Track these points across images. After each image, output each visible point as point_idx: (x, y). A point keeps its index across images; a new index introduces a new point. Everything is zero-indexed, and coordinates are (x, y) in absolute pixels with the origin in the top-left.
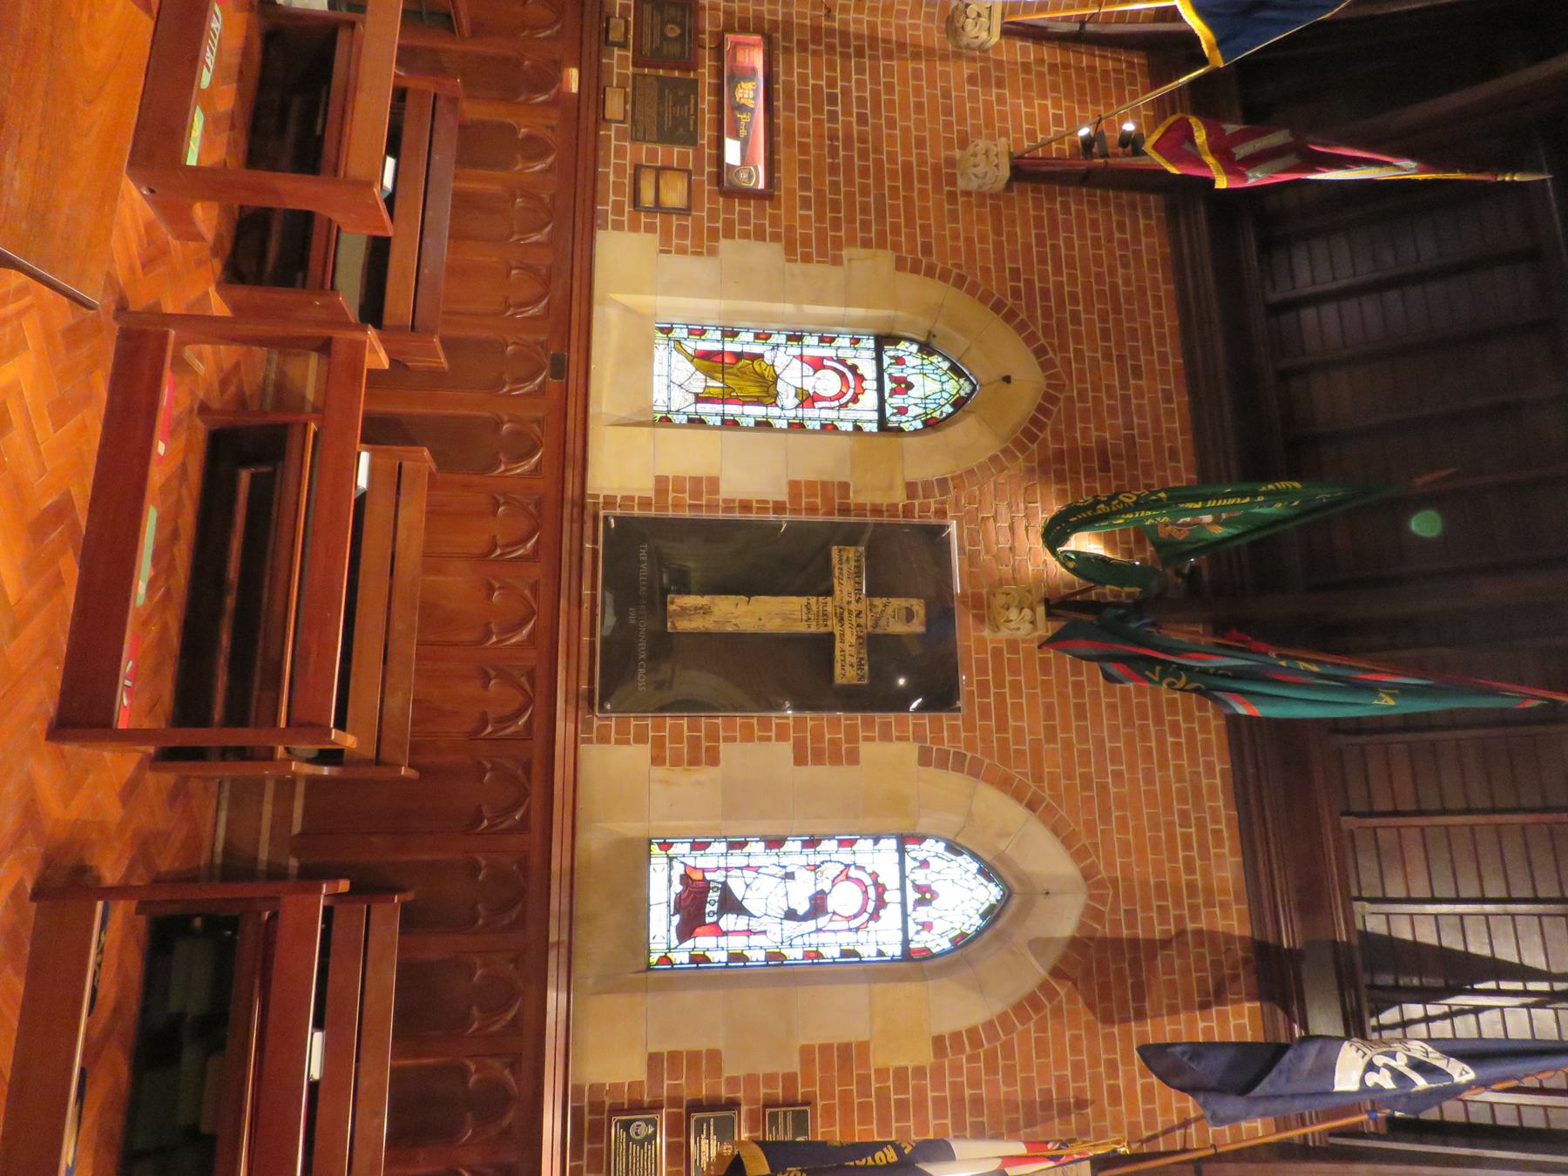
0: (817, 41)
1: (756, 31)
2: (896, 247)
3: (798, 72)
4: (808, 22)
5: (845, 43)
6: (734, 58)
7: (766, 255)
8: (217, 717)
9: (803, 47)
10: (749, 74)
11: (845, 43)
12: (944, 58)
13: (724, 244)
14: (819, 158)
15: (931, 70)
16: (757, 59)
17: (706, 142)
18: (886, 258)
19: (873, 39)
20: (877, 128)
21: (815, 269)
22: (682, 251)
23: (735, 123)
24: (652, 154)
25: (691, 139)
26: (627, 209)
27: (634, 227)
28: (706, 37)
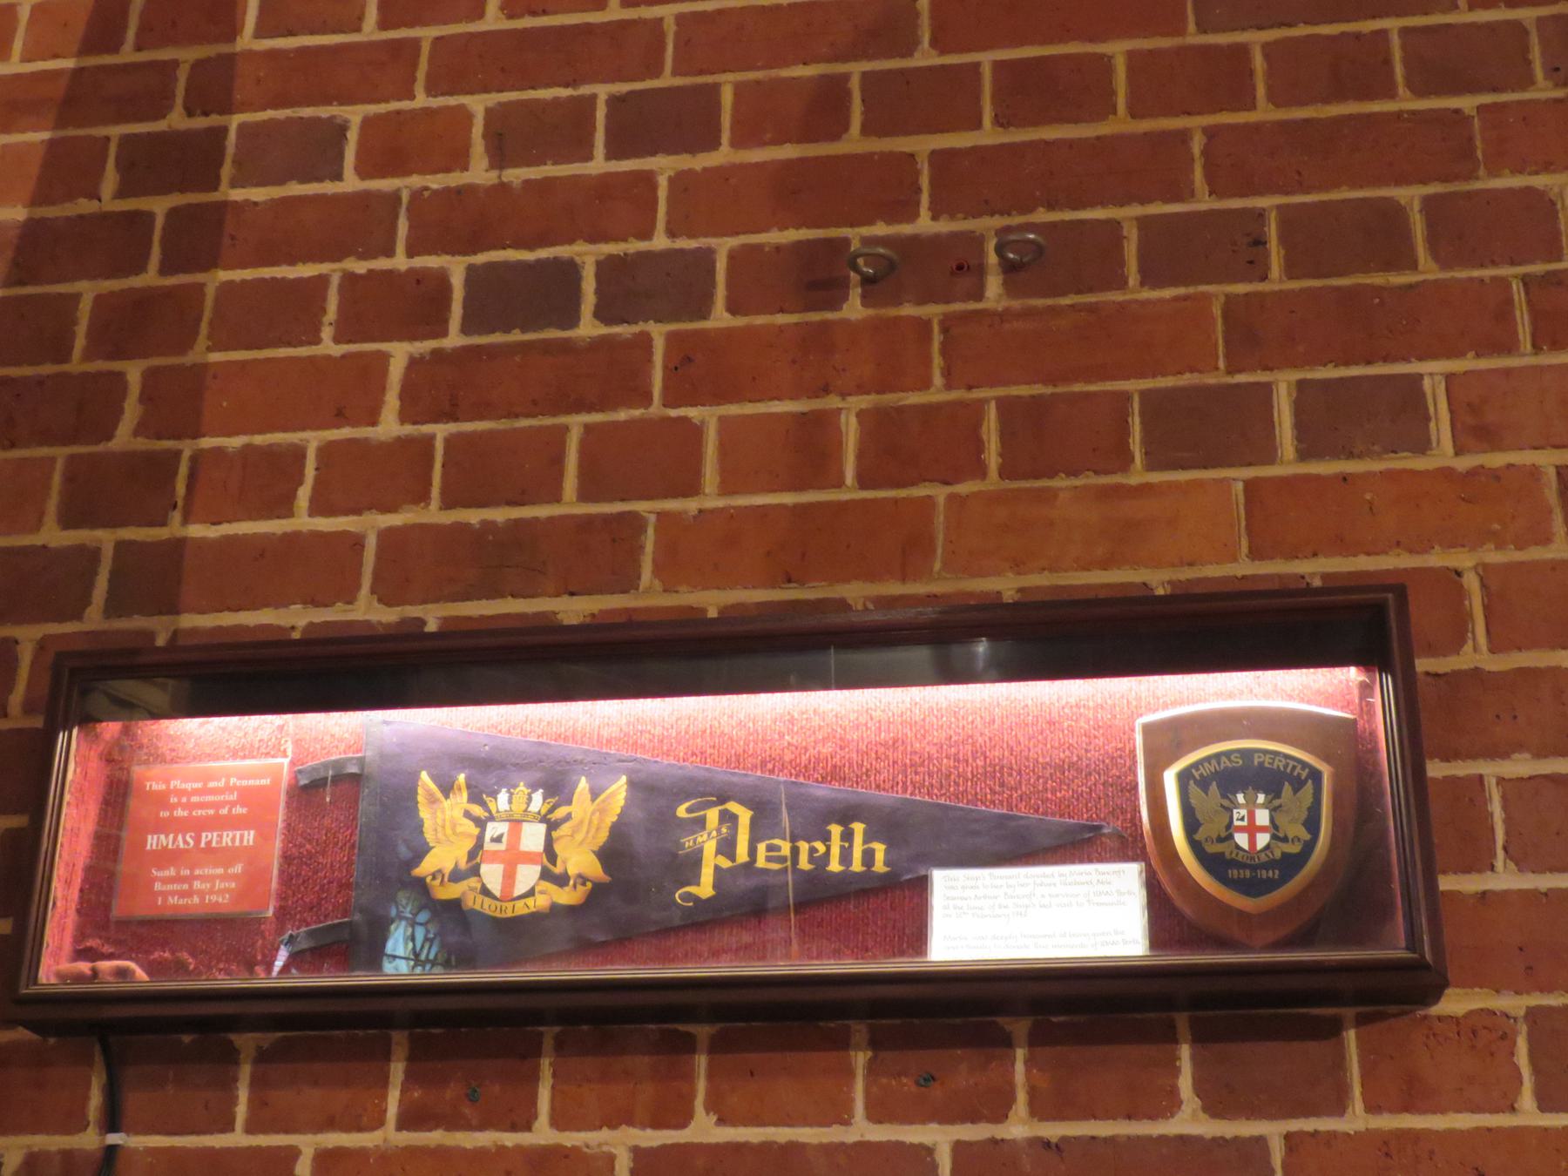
6: (519, 933)
9: (141, 486)
10: (349, 833)
16: (229, 765)
23: (823, 901)
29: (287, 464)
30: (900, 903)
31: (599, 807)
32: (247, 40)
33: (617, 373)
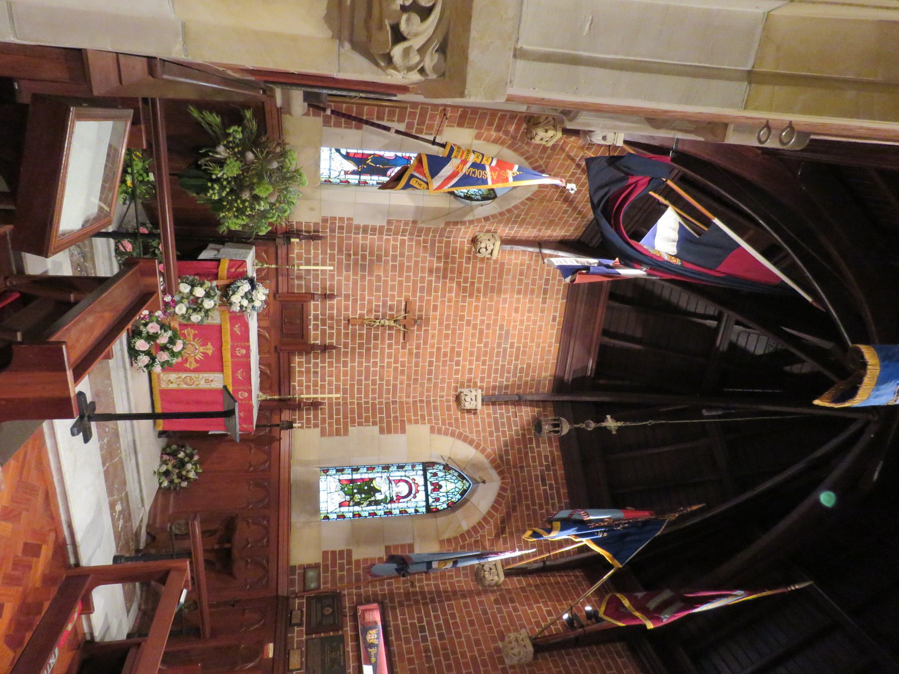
1: (374, 601)
5: (424, 598)
10: (373, 625)
11: (424, 598)
12: (479, 594)
16: (376, 616)
29: (517, 616)
30: (368, 662)
31: (376, 642)
32: (446, 603)
33: (416, 637)
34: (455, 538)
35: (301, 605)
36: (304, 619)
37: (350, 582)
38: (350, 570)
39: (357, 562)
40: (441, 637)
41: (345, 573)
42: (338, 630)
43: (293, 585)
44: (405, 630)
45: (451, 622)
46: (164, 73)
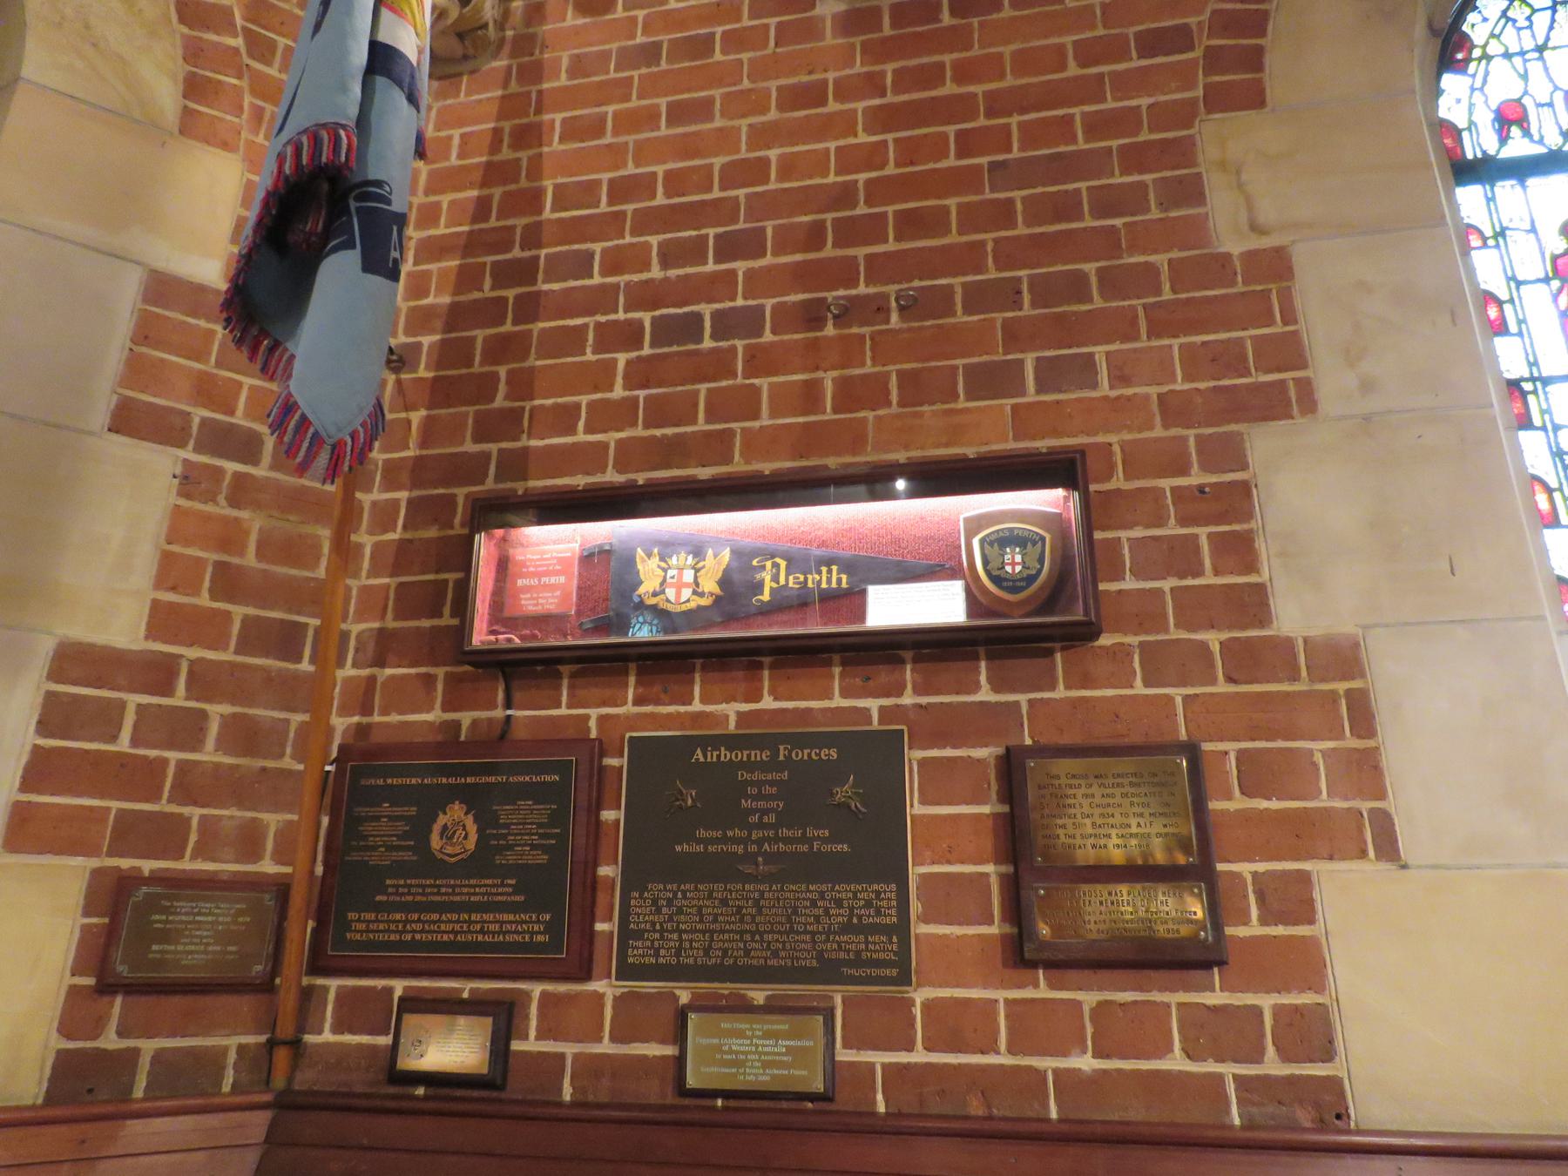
0: (486, 386)
1: (462, 556)
2: (1184, 115)
3: (588, 413)
4: (417, 417)
5: (492, 311)
6: (543, 621)
7: (1301, 488)
8: (210, 569)
9: (508, 424)
10: (606, 575)
11: (492, 311)
12: (532, 72)
13: (1292, 617)
14: (884, 347)
15: (567, 98)
16: (552, 546)
17: (873, 705)
18: (1221, 139)
19: (472, 244)
20: (764, 206)
21: (1320, 326)
22: (1365, 770)
24: (950, 898)
25: (876, 755)
26: (1216, 998)
27: (1306, 964)
28: (466, 718)
30: (853, 600)
31: (717, 562)
32: (547, 214)
33: (720, 364)
34: (193, 52)
35: (354, 1013)
36: (465, 988)
37: (288, 691)
38: (205, 682)
39: (162, 621)
40: (747, 245)
41: (217, 711)
42: (601, 774)
43: (211, 1062)
44: (659, 413)
45: (660, 199)
46: (219, 1093)
